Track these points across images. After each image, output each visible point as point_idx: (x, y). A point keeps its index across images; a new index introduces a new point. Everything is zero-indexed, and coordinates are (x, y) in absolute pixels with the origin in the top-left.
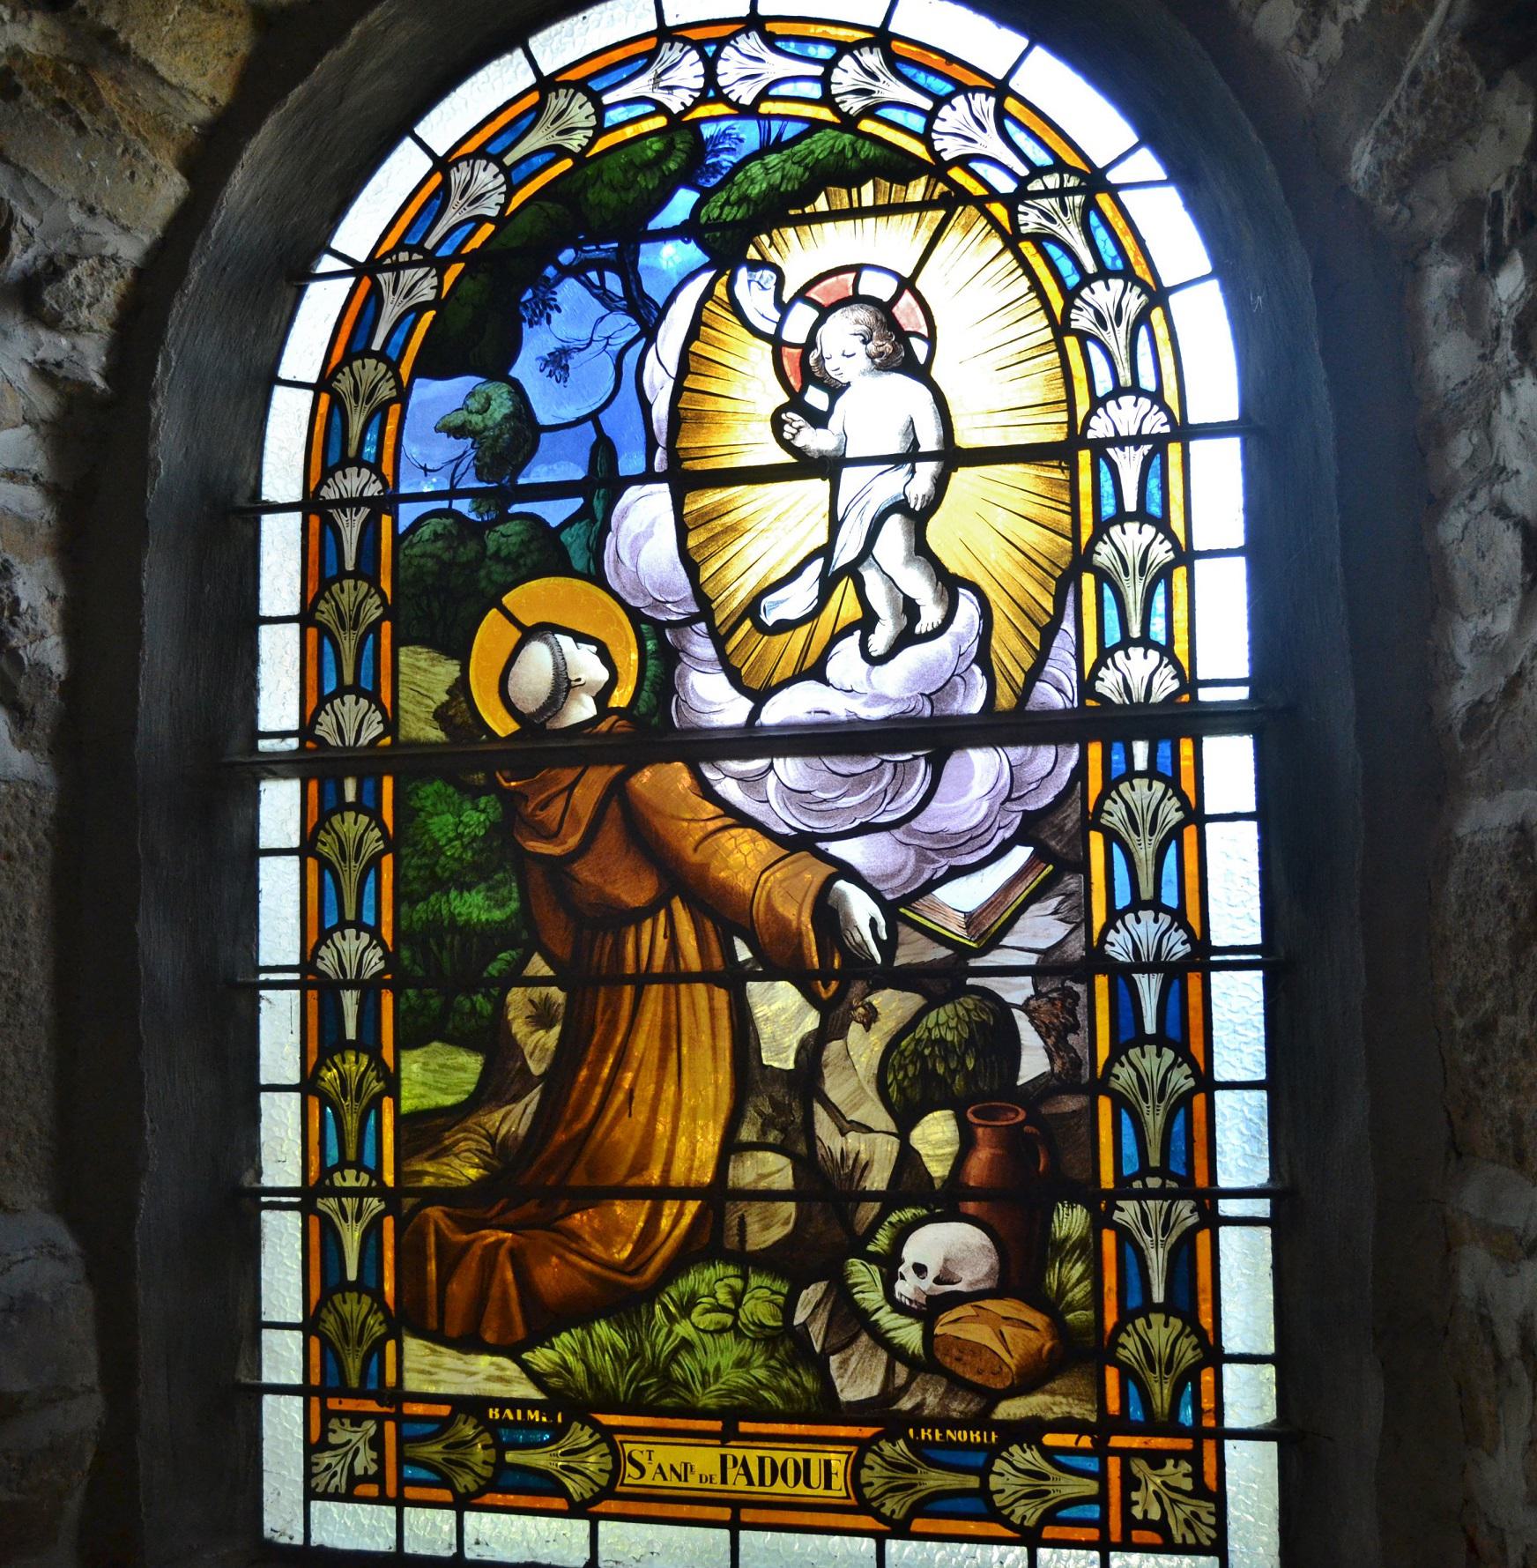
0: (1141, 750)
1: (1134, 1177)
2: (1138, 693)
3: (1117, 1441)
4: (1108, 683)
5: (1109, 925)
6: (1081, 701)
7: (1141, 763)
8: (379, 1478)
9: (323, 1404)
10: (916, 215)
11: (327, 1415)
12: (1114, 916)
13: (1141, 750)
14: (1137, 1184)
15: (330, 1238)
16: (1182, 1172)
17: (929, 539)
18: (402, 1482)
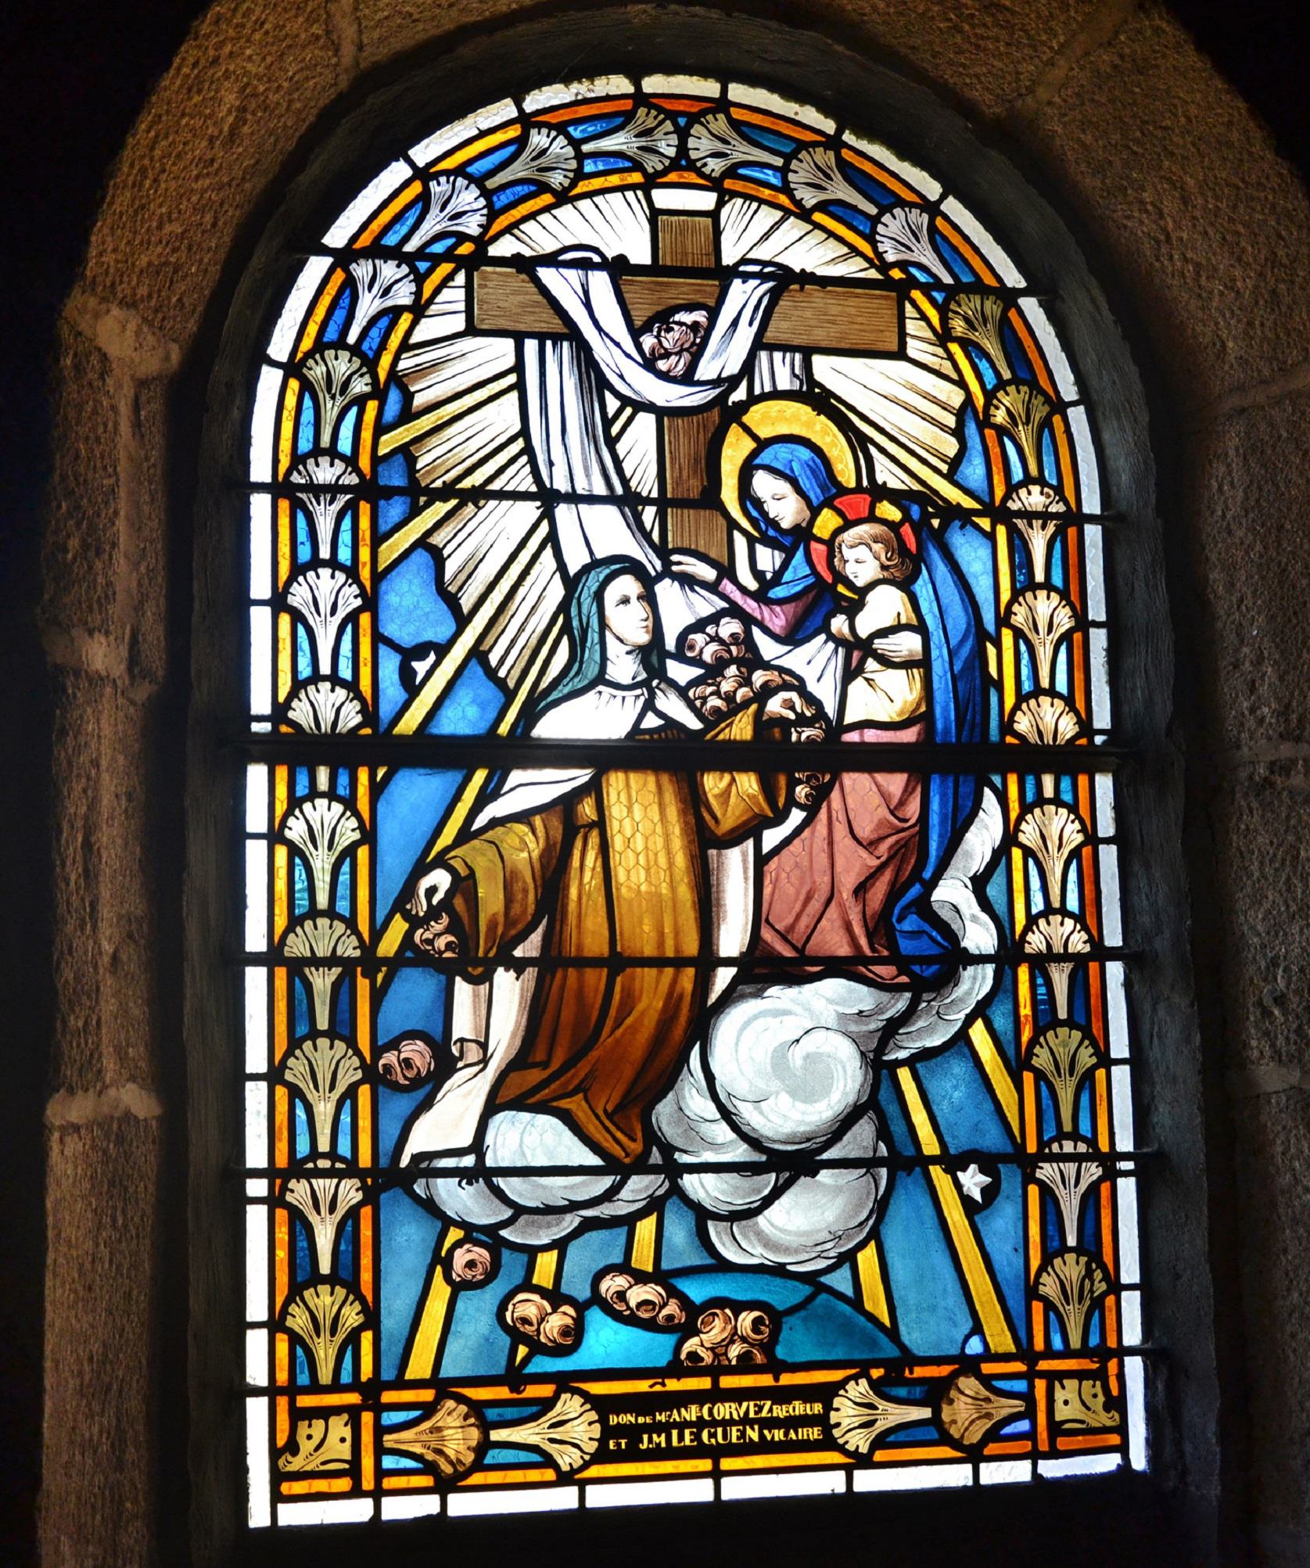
0: (1048, 781)
1: (306, 1160)
2: (1048, 739)
3: (1043, 1365)
4: (300, 712)
5: (1028, 928)
6: (1003, 738)
7: (1049, 792)
8: (353, 1470)
9: (292, 1403)
10: (908, 339)
11: (298, 1415)
12: (1032, 920)
13: (1048, 781)
14: (310, 1165)
15: (1050, 1208)
16: (348, 1155)
17: (563, 592)
18: (380, 1473)
